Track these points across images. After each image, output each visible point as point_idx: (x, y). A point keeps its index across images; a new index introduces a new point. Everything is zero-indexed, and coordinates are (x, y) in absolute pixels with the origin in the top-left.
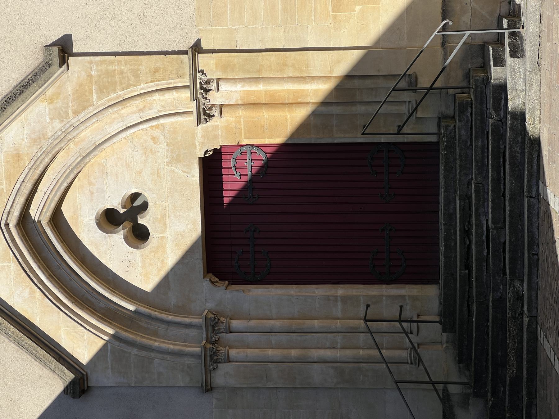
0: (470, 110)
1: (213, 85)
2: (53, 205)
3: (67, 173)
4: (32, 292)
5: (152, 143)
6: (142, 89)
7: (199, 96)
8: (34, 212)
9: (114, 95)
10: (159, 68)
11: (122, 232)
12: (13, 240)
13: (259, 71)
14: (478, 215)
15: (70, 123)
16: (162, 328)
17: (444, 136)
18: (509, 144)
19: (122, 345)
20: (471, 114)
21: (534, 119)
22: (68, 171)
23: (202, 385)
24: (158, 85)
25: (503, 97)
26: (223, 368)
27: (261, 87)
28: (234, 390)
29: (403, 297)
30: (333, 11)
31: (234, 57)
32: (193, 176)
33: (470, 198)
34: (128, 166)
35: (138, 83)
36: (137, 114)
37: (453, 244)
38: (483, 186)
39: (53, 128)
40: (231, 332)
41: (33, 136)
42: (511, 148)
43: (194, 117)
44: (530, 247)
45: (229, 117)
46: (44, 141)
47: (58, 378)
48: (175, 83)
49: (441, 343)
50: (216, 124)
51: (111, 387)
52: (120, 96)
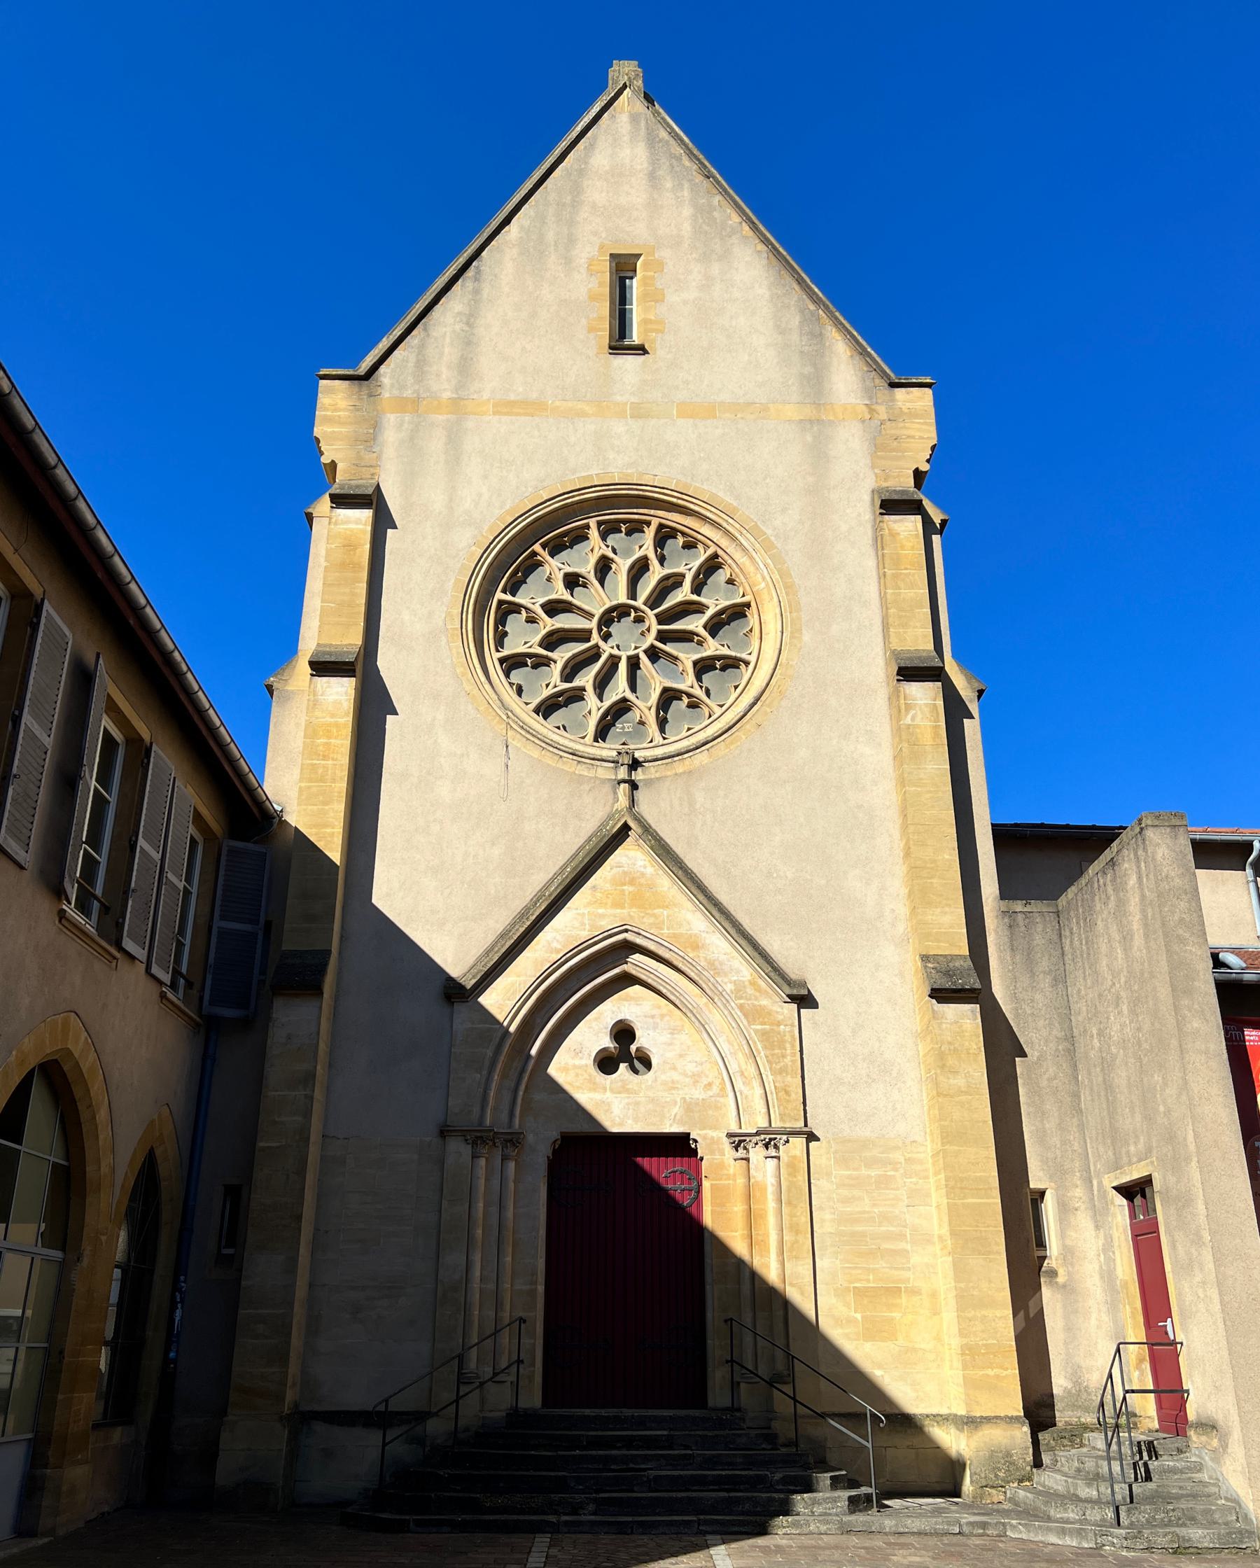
0: (769, 1447)
1: (772, 1152)
2: (643, 977)
3: (676, 993)
4: (558, 951)
5: (706, 1082)
6: (767, 1076)
7: (763, 1137)
8: (637, 957)
9: (760, 1046)
10: (789, 1096)
11: (612, 1046)
15: (730, 1001)
17: (732, 1416)
18: (753, 1497)
19: (498, 1040)
20: (764, 1449)
21: (788, 1527)
22: (678, 995)
23: (449, 1126)
24: (772, 1093)
25: (798, 1488)
26: (466, 1150)
27: (771, 1204)
28: (441, 1162)
30: (854, 1288)
31: (804, 1177)
32: (671, 1125)
33: (671, 1448)
34: (681, 1056)
35: (774, 1072)
36: (738, 1069)
37: (610, 1426)
38: (691, 1464)
39: (726, 983)
40: (502, 1160)
41: (716, 963)
43: (734, 1128)
44: (641, 1524)
45: (734, 1168)
46: (712, 973)
47: (464, 972)
48: (775, 1111)
49: (481, 1411)
50: (726, 1153)
51: (452, 1027)
52: (759, 1053)
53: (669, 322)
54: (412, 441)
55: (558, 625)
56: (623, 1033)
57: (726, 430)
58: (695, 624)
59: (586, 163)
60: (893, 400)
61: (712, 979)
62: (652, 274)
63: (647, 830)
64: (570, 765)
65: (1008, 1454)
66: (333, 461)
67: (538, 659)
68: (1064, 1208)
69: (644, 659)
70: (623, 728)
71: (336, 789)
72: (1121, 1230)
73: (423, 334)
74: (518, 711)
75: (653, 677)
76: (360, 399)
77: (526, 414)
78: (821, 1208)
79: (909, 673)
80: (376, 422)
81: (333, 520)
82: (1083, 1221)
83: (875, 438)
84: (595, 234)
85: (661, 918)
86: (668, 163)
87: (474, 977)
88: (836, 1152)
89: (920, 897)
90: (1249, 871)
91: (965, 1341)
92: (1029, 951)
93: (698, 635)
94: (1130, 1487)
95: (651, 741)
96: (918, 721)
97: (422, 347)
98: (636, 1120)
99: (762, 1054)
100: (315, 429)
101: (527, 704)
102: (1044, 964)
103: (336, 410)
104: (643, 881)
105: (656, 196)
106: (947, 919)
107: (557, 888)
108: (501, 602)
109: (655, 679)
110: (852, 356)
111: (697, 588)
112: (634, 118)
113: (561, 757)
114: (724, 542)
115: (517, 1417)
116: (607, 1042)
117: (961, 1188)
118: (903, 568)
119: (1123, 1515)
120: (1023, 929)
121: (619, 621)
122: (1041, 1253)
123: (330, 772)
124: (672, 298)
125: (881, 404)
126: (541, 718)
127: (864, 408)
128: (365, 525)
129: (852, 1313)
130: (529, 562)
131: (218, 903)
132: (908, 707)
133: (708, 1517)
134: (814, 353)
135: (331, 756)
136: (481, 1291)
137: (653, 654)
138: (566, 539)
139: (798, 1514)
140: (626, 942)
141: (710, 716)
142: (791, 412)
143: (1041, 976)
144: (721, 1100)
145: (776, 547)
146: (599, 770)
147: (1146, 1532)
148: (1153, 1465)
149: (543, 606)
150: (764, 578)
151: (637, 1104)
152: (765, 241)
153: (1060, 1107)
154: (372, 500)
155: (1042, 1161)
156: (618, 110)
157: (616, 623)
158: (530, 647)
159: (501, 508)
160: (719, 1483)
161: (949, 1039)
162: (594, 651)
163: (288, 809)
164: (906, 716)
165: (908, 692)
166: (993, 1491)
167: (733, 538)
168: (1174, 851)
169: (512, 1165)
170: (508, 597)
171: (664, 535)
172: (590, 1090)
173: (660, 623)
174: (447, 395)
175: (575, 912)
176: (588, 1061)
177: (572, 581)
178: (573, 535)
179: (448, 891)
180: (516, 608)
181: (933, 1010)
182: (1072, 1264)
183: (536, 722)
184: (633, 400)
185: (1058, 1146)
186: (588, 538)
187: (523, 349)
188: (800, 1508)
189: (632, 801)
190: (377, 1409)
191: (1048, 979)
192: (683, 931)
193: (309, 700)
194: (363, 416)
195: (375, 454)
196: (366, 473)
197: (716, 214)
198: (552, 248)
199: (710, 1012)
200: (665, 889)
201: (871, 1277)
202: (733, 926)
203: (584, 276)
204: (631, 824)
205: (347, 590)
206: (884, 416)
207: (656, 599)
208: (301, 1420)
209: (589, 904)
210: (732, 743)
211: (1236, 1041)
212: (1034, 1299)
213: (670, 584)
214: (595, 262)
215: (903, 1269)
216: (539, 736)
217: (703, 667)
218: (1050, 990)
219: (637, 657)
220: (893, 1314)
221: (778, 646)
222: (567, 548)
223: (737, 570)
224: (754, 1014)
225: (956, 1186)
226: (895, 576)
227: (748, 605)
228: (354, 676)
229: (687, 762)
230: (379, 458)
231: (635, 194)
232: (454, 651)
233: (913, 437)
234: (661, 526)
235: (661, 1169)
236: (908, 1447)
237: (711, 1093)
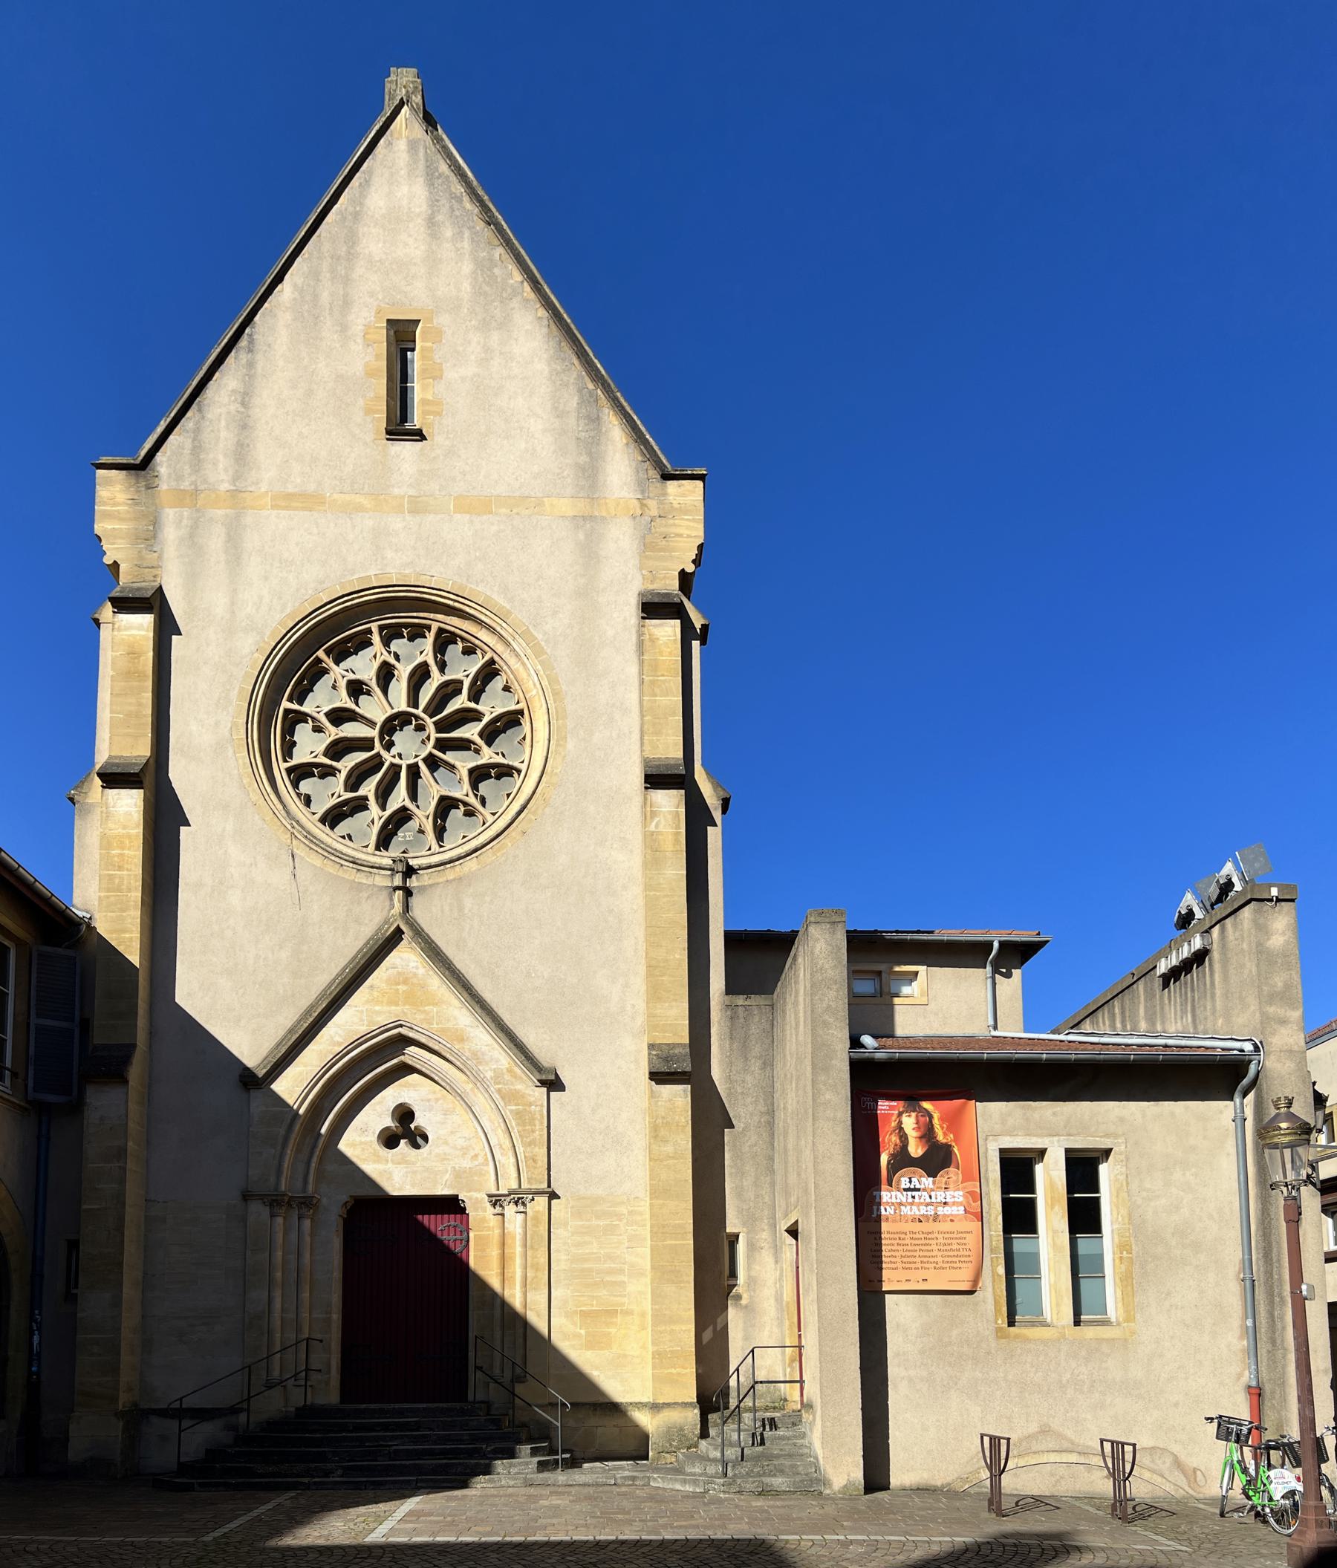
0: (495, 1428)
1: (521, 1208)
2: (418, 1067)
4: (340, 1044)
5: (473, 1154)
7: (512, 1196)
9: (514, 1124)
11: (393, 1125)
13: (532, 1247)
19: (289, 1121)
26: (265, 1212)
27: (519, 1250)
29: (329, 1372)
32: (442, 1189)
34: (452, 1133)
35: (525, 1145)
40: (299, 1219)
41: (479, 1053)
45: (494, 1222)
52: (513, 1129)
53: (448, 404)
54: (192, 538)
55: (342, 735)
56: (404, 1114)
57: (502, 527)
58: (471, 731)
59: (361, 204)
60: (665, 494)
61: (475, 1068)
62: (430, 344)
63: (419, 934)
64: (350, 873)
65: (682, 1429)
66: (115, 561)
67: (325, 769)
68: (752, 1247)
69: (424, 769)
70: (405, 837)
71: (132, 899)
72: (788, 1263)
73: (198, 416)
74: (304, 820)
75: (431, 786)
76: (138, 492)
77: (303, 509)
78: (558, 1251)
79: (656, 779)
80: (155, 517)
81: (116, 626)
82: (766, 1257)
83: (644, 537)
84: (372, 294)
85: (431, 1014)
86: (447, 206)
87: (264, 1067)
88: (572, 1207)
89: (655, 994)
90: (989, 968)
91: (655, 1348)
92: (746, 1038)
93: (474, 744)
94: (743, 1450)
95: (430, 849)
96: (661, 828)
97: (198, 430)
98: (413, 1185)
99: (516, 1130)
100: (96, 526)
101: (314, 814)
102: (756, 1050)
103: (114, 505)
104: (415, 981)
105: (434, 248)
106: (673, 1012)
107: (336, 987)
108: (287, 711)
109: (433, 789)
110: (627, 444)
111: (476, 695)
112: (413, 145)
113: (342, 865)
114: (500, 648)
115: (308, 1412)
116: (388, 1122)
117: (663, 1233)
119: (729, 1469)
120: (742, 1020)
121: (401, 730)
122: (731, 1282)
123: (125, 882)
124: (451, 374)
125: (653, 499)
126: (327, 829)
127: (636, 502)
128: (147, 631)
129: (578, 1330)
130: (314, 669)
131: (33, 1003)
132: (654, 814)
133: (424, 1477)
134: (590, 440)
135: (126, 866)
136: (282, 1319)
137: (433, 763)
138: (349, 645)
139: (498, 1474)
140: (400, 1035)
141: (484, 824)
142: (566, 506)
143: (753, 1061)
144: (485, 1168)
145: (546, 653)
146: (377, 878)
147: (739, 1481)
148: (768, 1434)
149: (328, 715)
150: (535, 685)
151: (415, 1172)
152: (548, 304)
153: (757, 1169)
154: (154, 603)
155: (738, 1212)
156: (396, 135)
157: (398, 732)
158: (316, 757)
159: (282, 611)
160: (444, 1453)
161: (663, 1114)
162: (377, 760)
163: (97, 916)
164: (651, 822)
165: (654, 799)
166: (668, 1455)
167: (508, 644)
168: (831, 945)
169: (307, 1223)
170: (295, 707)
171: (444, 641)
172: (374, 1162)
173: (438, 731)
174: (225, 486)
175: (354, 1009)
176: (373, 1138)
177: (356, 689)
178: (357, 640)
179: (241, 991)
180: (302, 717)
181: (652, 1090)
182: (754, 1291)
183: (322, 832)
184: (410, 494)
185: (753, 1199)
186: (372, 644)
187: (300, 434)
188: (500, 1470)
189: (406, 907)
190: (171, 1406)
191: (759, 1063)
192: (450, 1025)
193: (102, 812)
194: (143, 511)
195: (155, 554)
196: (148, 574)
197: (496, 271)
198: (327, 311)
199: (475, 1096)
200: (435, 988)
201: (595, 1302)
202: (493, 1021)
203: (361, 347)
204: (404, 928)
205: (133, 700)
206: (654, 512)
207: (435, 707)
208: (137, 1417)
209: (368, 1002)
210: (499, 850)
211: (870, 1110)
212: (721, 1317)
213: (449, 690)
214: (371, 331)
215: (620, 1296)
216: (322, 845)
217: (478, 775)
218: (760, 1072)
219: (416, 765)
220: (610, 1330)
221: (545, 754)
222: (351, 654)
223: (512, 676)
224: (510, 1097)
225: (659, 1230)
226: (652, 682)
227: (521, 712)
228: (142, 788)
229: (457, 869)
230: (160, 558)
231: (413, 244)
232: (240, 761)
233: (680, 535)
234: (441, 631)
235: (438, 1224)
236: (614, 1426)
237: (476, 1163)
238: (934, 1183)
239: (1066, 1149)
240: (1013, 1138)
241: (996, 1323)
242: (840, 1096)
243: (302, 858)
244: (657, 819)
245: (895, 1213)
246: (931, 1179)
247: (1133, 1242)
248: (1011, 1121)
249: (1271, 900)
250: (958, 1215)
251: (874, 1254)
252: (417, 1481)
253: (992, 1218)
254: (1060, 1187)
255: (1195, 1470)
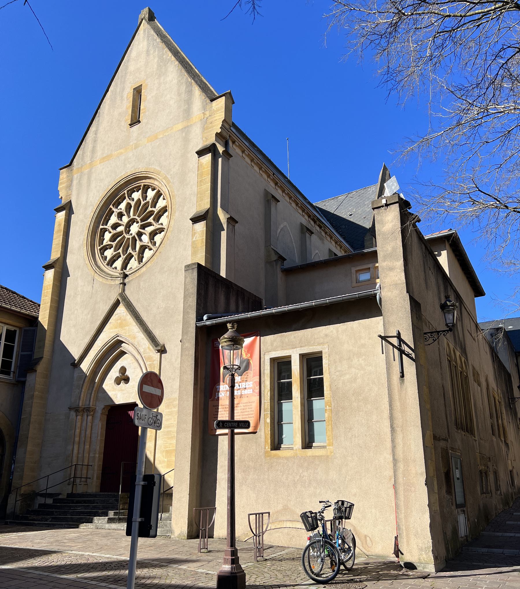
12: (114, 339)
14: (82, 506)
16: (90, 391)
29: (93, 479)
42: (84, 518)
56: (123, 370)
108: (101, 229)
118: (203, 177)
129: (164, 459)
130: (110, 212)
169: (90, 418)
201: (171, 446)
238: (241, 379)
239: (299, 354)
240: (276, 352)
241: (265, 448)
242: (191, 344)
243: (97, 280)
244: (196, 235)
245: (225, 395)
246: (240, 377)
247: (332, 400)
248: (275, 344)
249: (383, 206)
250: (250, 394)
251: (214, 416)
252: (65, 524)
253: (266, 393)
254: (297, 374)
255: (366, 536)
